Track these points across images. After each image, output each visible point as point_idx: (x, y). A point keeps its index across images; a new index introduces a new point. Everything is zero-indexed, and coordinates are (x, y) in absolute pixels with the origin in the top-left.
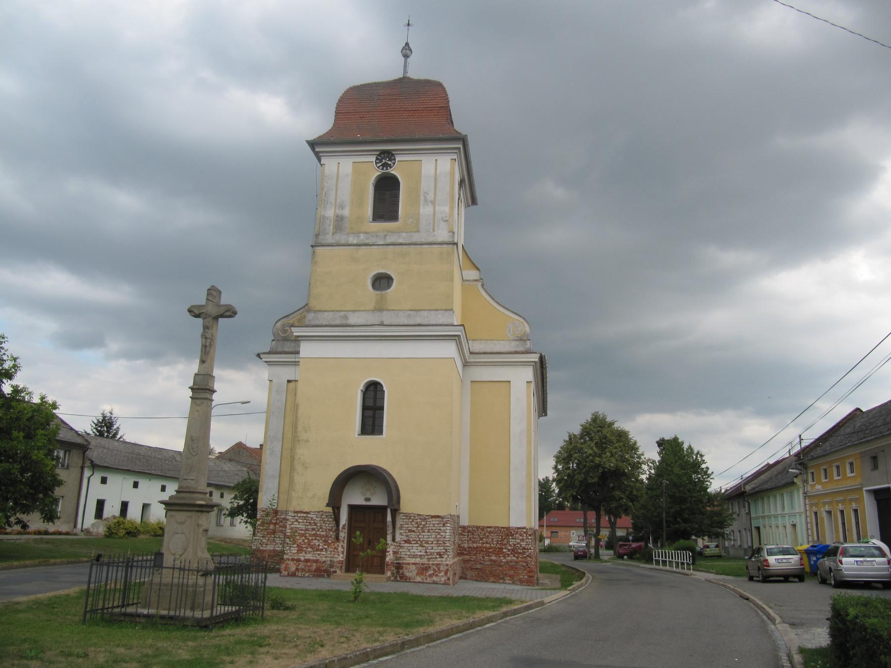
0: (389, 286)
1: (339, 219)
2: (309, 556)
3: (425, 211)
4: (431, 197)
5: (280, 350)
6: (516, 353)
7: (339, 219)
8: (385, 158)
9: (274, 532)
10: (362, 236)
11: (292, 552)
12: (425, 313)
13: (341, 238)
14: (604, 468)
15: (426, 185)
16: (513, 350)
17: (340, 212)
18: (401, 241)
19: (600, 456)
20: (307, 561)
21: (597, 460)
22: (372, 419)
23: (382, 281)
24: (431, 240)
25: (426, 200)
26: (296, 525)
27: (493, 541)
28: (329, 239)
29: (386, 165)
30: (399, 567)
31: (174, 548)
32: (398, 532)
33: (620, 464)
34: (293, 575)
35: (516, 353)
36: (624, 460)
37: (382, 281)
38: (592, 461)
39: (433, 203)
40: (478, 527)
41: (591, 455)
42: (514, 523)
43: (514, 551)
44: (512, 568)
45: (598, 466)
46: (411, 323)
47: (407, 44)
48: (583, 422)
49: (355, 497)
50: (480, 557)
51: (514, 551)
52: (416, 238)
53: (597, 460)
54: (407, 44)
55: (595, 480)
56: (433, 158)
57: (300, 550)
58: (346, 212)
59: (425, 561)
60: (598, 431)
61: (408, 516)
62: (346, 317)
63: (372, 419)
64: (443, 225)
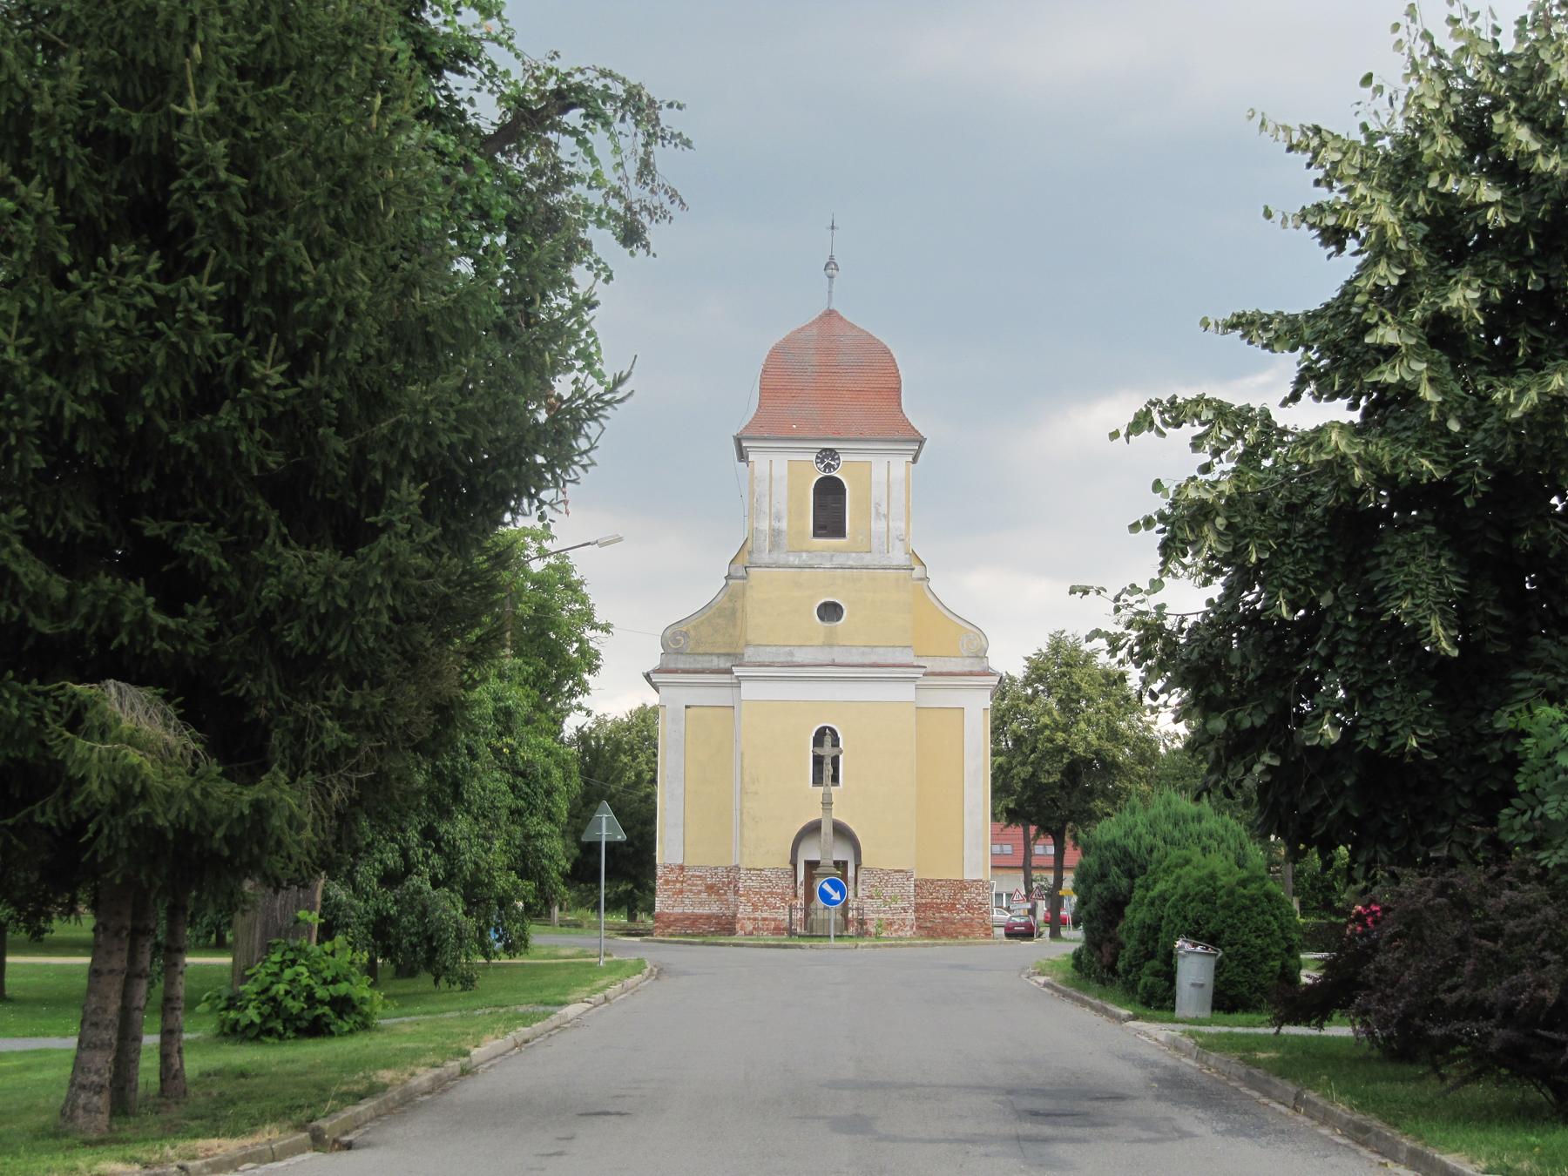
0: (839, 618)
1: (776, 534)
2: (765, 915)
3: (878, 526)
4: (883, 509)
5: (672, 666)
6: (971, 674)
7: (776, 534)
8: (828, 456)
9: (681, 892)
10: (804, 555)
11: (744, 911)
12: (881, 650)
13: (780, 557)
14: (1072, 753)
15: (878, 493)
16: (966, 669)
17: (776, 525)
18: (851, 563)
19: (1066, 729)
20: (764, 919)
21: (1060, 737)
22: (825, 769)
23: (830, 611)
24: (885, 563)
25: (878, 514)
26: (749, 883)
27: (945, 895)
28: (765, 558)
29: (829, 466)
30: (862, 923)
31: (1422, 849)
32: (860, 887)
33: (1108, 745)
34: (751, 934)
35: (971, 674)
36: (1114, 735)
37: (830, 611)
38: (1051, 740)
39: (887, 516)
40: (926, 881)
41: (1046, 726)
42: (967, 877)
43: (969, 907)
44: (966, 925)
45: (1064, 749)
46: (867, 661)
47: (831, 257)
48: (1031, 652)
49: (820, 850)
50: (929, 914)
51: (969, 907)
52: (867, 559)
53: (1060, 737)
54: (831, 257)
55: (1056, 777)
56: (886, 459)
57: (755, 908)
58: (784, 525)
59: (889, 916)
60: (1064, 675)
61: (870, 871)
62: (791, 654)
63: (825, 769)
64: (898, 544)
